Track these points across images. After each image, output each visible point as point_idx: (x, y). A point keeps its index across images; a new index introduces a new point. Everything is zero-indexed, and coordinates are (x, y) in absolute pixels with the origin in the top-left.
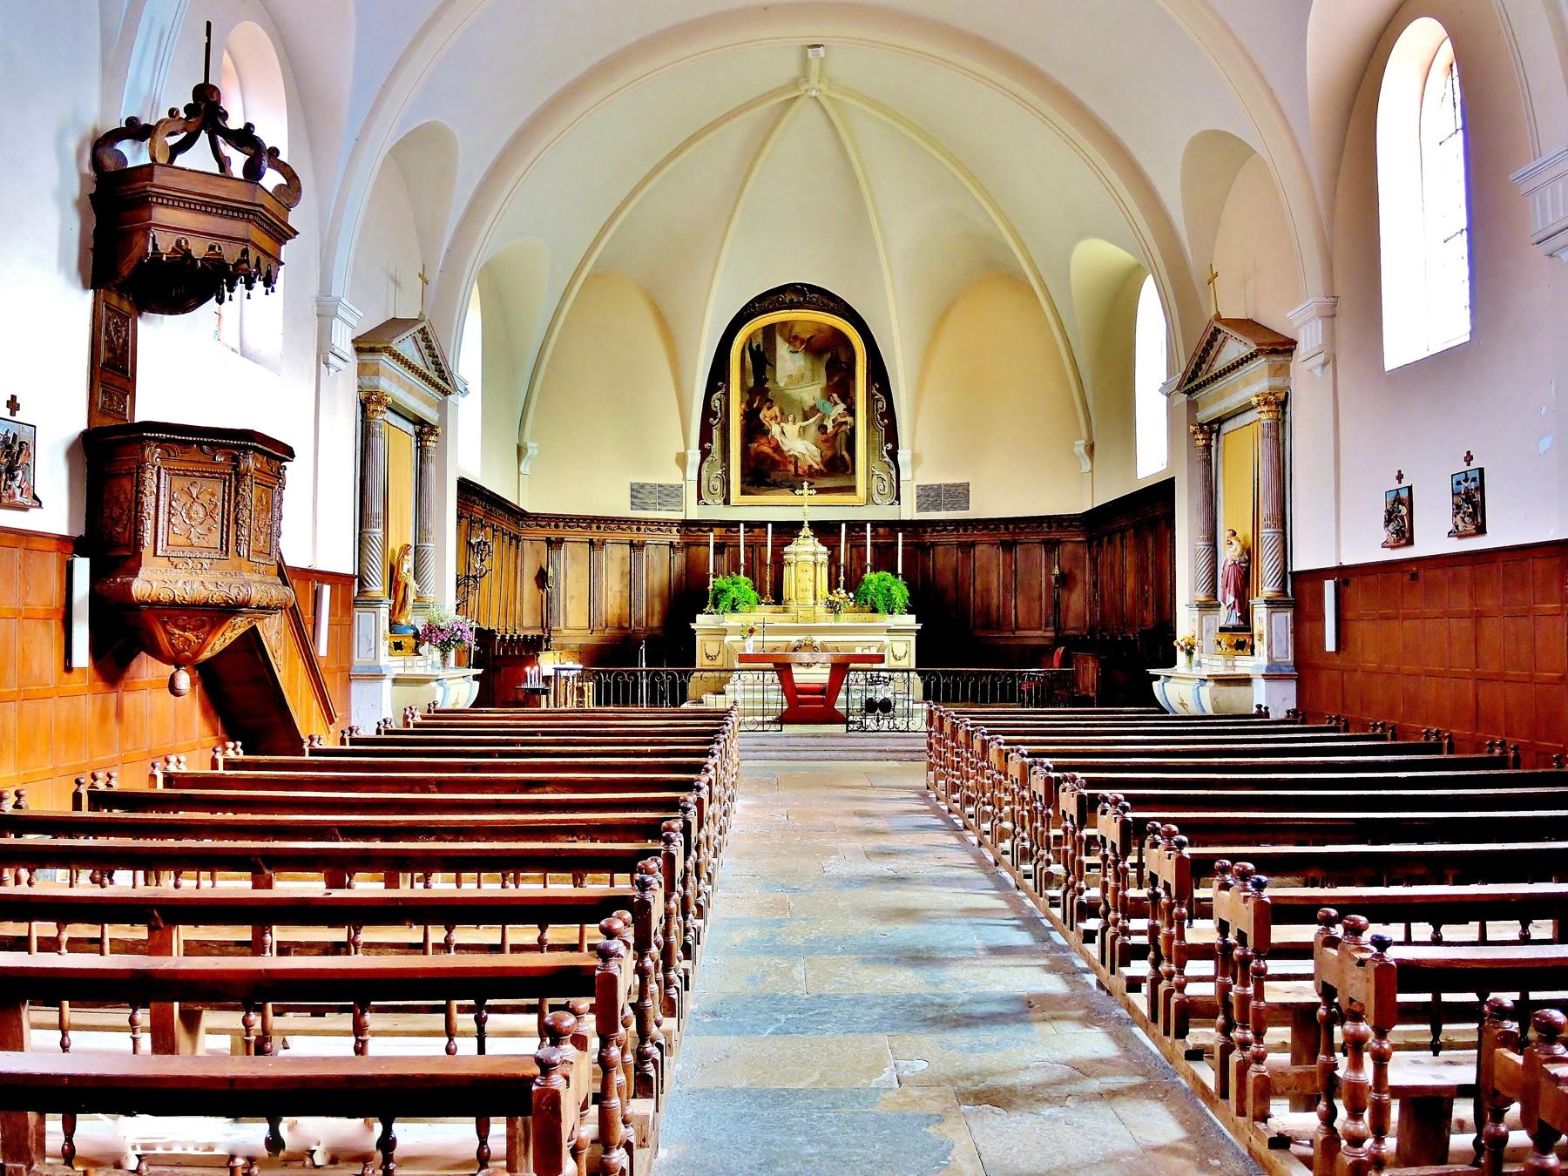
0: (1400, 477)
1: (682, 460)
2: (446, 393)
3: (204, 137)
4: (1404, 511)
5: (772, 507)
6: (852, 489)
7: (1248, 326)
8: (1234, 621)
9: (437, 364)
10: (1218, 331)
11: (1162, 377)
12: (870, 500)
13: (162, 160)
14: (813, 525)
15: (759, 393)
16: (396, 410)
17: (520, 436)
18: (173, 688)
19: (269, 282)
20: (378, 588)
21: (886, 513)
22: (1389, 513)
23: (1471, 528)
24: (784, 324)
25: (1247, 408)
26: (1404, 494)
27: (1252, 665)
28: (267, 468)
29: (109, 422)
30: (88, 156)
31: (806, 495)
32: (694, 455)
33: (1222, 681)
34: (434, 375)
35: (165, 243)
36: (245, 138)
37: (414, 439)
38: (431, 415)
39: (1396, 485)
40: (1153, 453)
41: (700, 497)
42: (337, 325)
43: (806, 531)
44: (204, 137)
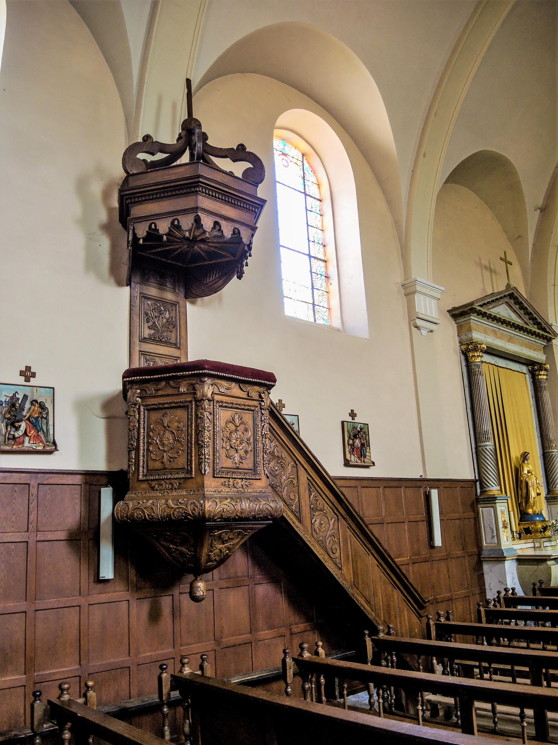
2: (549, 340)
9: (534, 319)
34: (534, 329)
37: (528, 376)
38: (539, 356)
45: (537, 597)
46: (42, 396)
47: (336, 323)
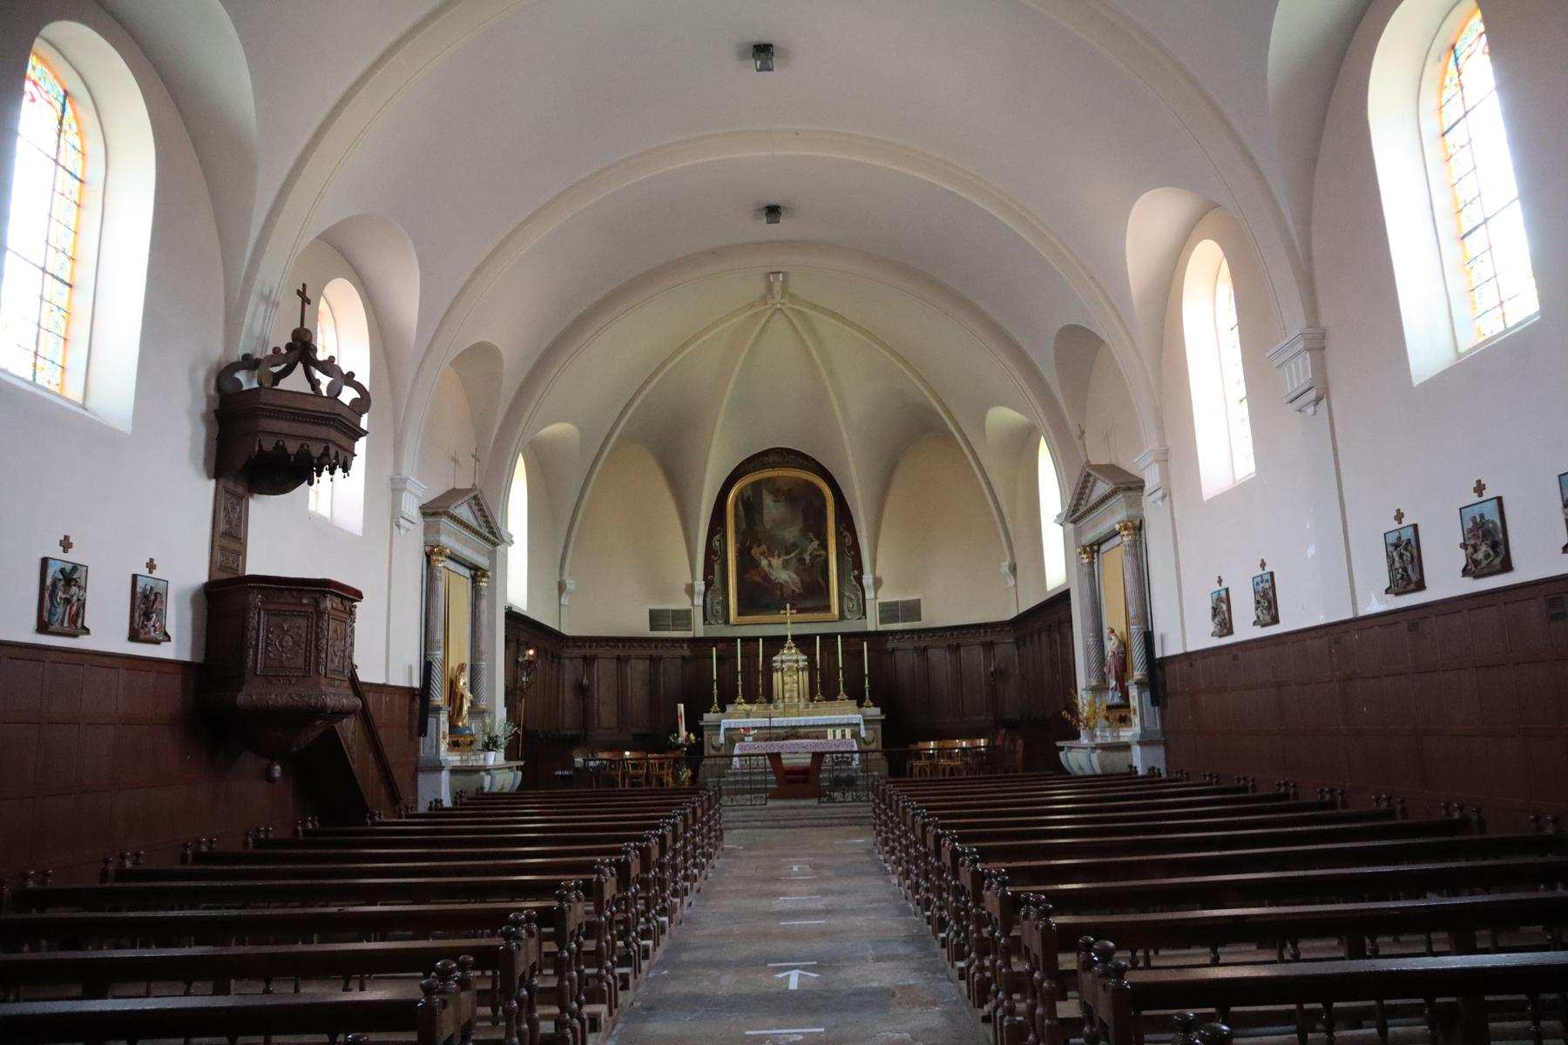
0: (1220, 581)
1: (690, 590)
2: (495, 544)
3: (300, 366)
4: (1224, 607)
5: (762, 626)
6: (828, 608)
7: (1111, 471)
8: (1117, 700)
9: (487, 522)
10: (1089, 475)
11: (1059, 510)
12: (842, 617)
13: (267, 385)
14: (794, 638)
15: (750, 535)
16: (454, 558)
17: (561, 575)
18: (268, 776)
19: (346, 469)
20: (439, 698)
21: (852, 625)
22: (1214, 609)
23: (1268, 618)
24: (769, 480)
25: (1115, 534)
26: (1223, 594)
27: (1128, 734)
28: (341, 607)
29: (224, 576)
30: (213, 382)
31: (789, 614)
32: (700, 585)
33: (1106, 748)
34: (485, 532)
35: (269, 444)
36: (329, 366)
38: (482, 561)
39: (1217, 588)
40: (1056, 571)
41: (705, 619)
42: (406, 497)
43: (790, 643)
44: (300, 366)
45: (107, 885)
46: (160, 588)
47: (74, 392)
